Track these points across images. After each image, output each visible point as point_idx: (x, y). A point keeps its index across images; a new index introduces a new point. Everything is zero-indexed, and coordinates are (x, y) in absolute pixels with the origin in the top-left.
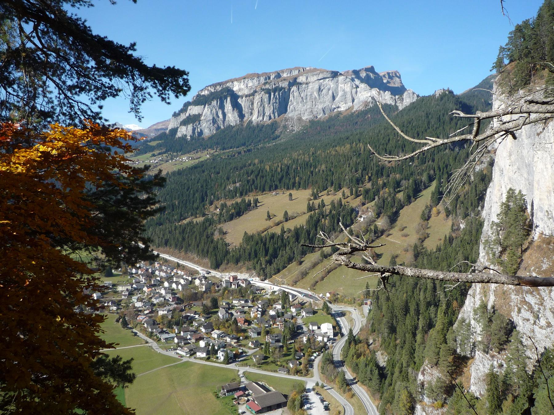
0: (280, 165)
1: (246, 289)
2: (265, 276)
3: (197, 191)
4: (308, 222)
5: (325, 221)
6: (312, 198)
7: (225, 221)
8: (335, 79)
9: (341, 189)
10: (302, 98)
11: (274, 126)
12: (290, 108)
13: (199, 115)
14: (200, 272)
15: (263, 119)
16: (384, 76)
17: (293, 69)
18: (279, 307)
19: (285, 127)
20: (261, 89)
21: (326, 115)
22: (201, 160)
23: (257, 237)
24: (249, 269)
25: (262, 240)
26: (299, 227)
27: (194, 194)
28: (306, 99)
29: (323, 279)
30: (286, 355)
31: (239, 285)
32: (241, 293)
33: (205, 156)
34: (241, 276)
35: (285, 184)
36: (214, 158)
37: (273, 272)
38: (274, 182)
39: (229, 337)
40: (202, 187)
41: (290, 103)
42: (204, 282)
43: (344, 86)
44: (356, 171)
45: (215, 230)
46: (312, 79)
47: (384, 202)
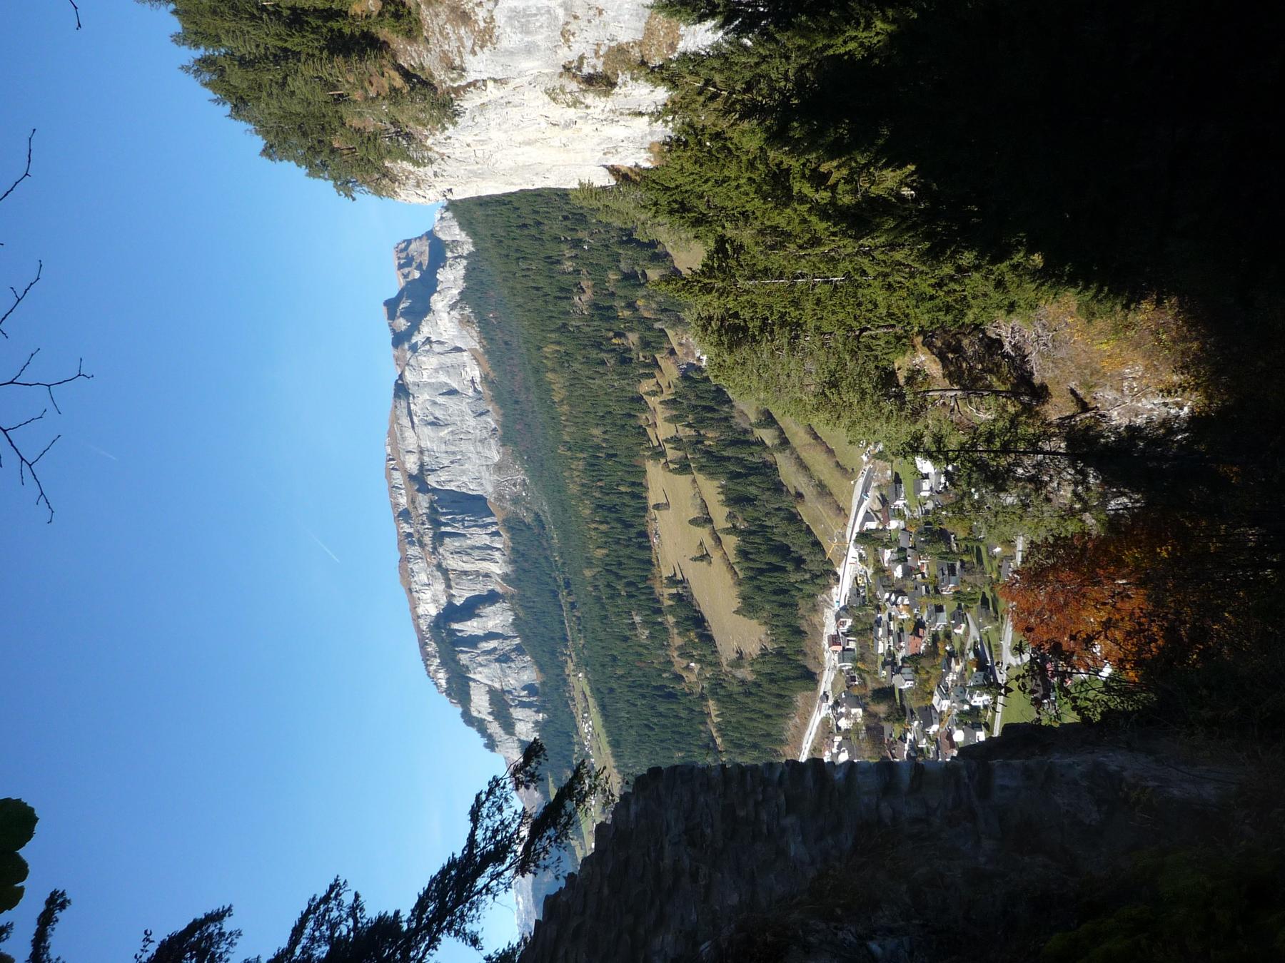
0: (594, 525)
1: (857, 619)
2: (828, 575)
3: (652, 708)
4: (712, 475)
5: (708, 439)
6: (663, 461)
7: (715, 652)
8: (412, 389)
9: (642, 398)
10: (452, 462)
11: (514, 526)
12: (474, 489)
13: (492, 691)
14: (823, 714)
15: (498, 549)
16: (405, 276)
17: (390, 482)
18: (887, 554)
19: (516, 500)
20: (433, 553)
21: (490, 408)
22: (588, 692)
23: (746, 588)
24: (815, 609)
25: (751, 579)
26: (722, 497)
27: (661, 715)
28: (454, 453)
29: (830, 452)
30: (980, 560)
31: (850, 632)
32: (865, 630)
33: (579, 682)
34: (830, 628)
35: (634, 516)
36: (583, 664)
37: (819, 557)
38: (630, 539)
39: (947, 674)
40: (644, 697)
41: (464, 490)
42: (843, 710)
43: (426, 370)
44: (603, 363)
45: (734, 677)
46: (411, 441)
47: (665, 310)
